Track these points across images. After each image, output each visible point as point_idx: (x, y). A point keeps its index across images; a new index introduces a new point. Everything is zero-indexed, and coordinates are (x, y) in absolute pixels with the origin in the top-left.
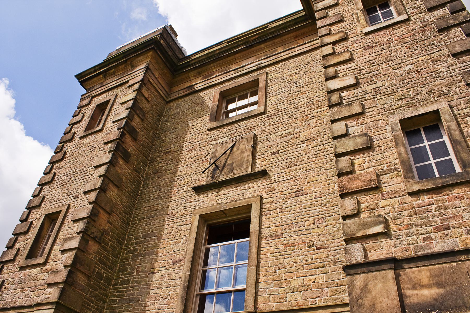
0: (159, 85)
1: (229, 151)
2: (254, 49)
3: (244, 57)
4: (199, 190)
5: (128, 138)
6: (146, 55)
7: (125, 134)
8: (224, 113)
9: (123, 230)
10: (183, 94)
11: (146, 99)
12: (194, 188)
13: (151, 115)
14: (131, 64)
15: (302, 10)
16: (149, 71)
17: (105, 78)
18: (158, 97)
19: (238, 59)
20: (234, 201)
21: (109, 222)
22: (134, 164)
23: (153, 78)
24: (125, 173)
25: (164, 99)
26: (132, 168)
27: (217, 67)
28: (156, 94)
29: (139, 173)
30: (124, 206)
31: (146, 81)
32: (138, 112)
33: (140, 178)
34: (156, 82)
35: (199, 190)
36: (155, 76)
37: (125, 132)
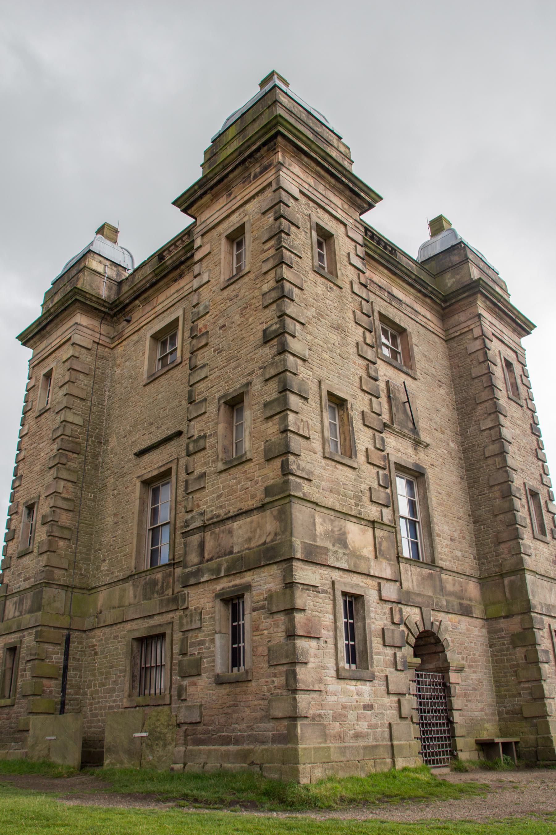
8: (159, 360)
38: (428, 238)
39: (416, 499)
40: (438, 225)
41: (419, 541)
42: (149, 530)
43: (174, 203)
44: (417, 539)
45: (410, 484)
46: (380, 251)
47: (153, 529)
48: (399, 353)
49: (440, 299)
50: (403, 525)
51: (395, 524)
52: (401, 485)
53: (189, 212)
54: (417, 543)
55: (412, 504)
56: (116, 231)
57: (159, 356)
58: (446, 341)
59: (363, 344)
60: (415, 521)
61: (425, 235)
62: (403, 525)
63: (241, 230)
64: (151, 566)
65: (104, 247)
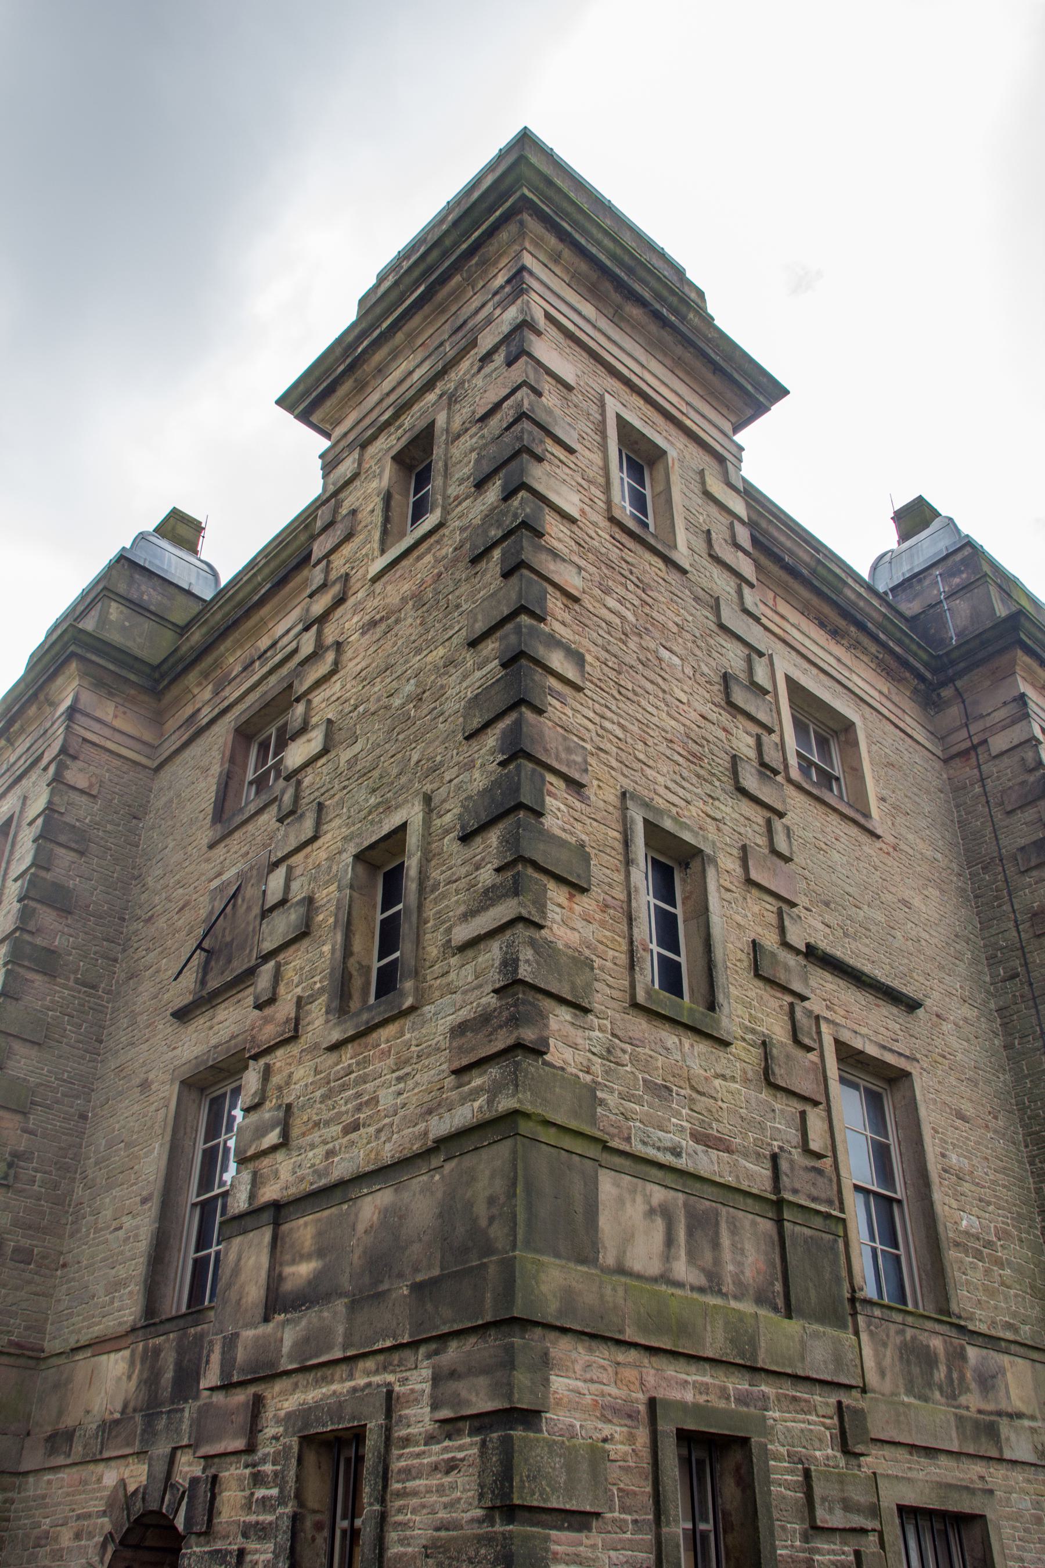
0: (118, 737)
1: (230, 906)
2: (292, 585)
3: (277, 613)
4: (183, 1015)
5: (47, 917)
6: (67, 673)
7: (34, 909)
8: (251, 783)
9: (71, 1135)
10: (178, 744)
11: (82, 792)
12: (173, 1015)
13: (109, 827)
14: (47, 700)
15: (204, 601)
16: (78, 716)
17: (12, 744)
18: (125, 768)
19: (271, 619)
20: (233, 1037)
21: (25, 1131)
22: (75, 972)
23: (96, 727)
24: (52, 1002)
25: (145, 767)
26: (71, 983)
27: (235, 651)
28: (117, 763)
29: (94, 987)
30: (64, 1081)
31: (74, 745)
32: (62, 839)
33: (100, 997)
34: (107, 732)
35: (183, 1015)
36: (99, 720)
37: (32, 904)
38: (894, 546)
39: (892, 1141)
40: (915, 517)
41: (902, 1252)
42: (194, 1205)
43: (279, 402)
44: (897, 1248)
45: (874, 1102)
46: (784, 556)
47: (203, 1204)
48: (837, 779)
49: (926, 665)
50: (858, 1216)
51: (842, 1210)
52: (849, 1107)
53: (314, 419)
54: (897, 1257)
55: (881, 1155)
56: (197, 528)
57: (250, 776)
58: (946, 761)
59: (706, 562)
60: (890, 1200)
61: (889, 539)
62: (858, 1216)
63: (424, 439)
64: (189, 1306)
65: (171, 561)
